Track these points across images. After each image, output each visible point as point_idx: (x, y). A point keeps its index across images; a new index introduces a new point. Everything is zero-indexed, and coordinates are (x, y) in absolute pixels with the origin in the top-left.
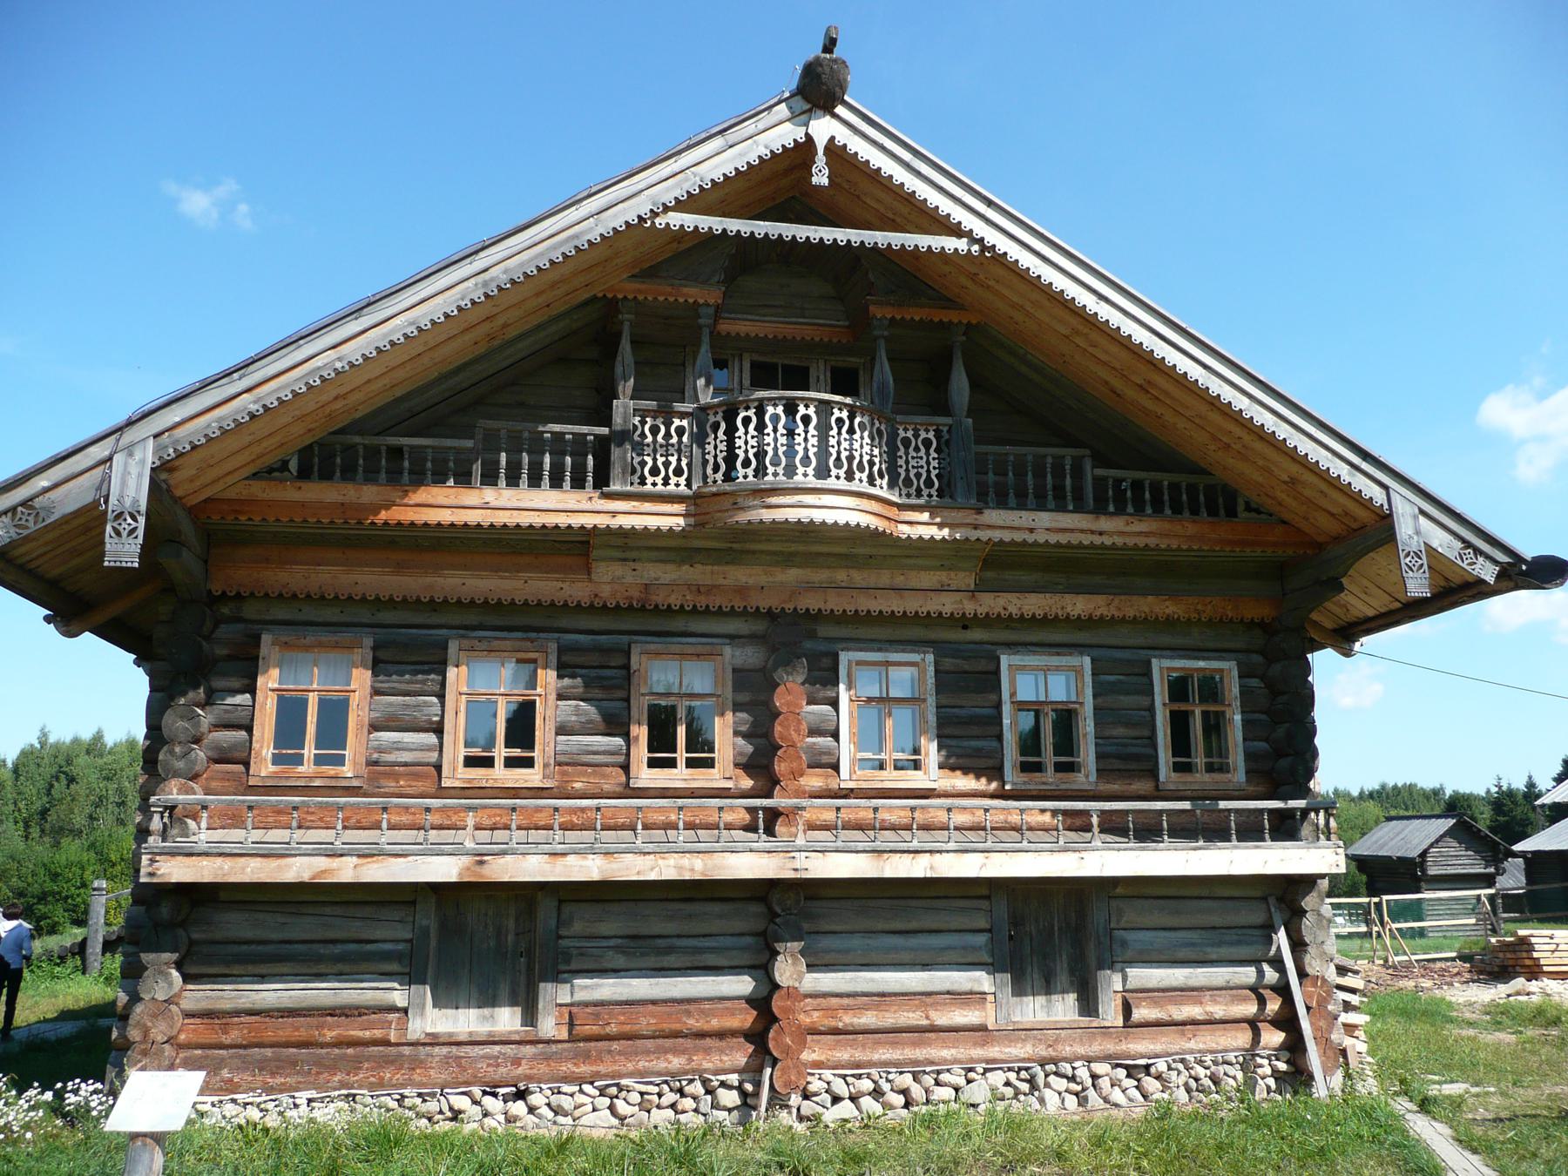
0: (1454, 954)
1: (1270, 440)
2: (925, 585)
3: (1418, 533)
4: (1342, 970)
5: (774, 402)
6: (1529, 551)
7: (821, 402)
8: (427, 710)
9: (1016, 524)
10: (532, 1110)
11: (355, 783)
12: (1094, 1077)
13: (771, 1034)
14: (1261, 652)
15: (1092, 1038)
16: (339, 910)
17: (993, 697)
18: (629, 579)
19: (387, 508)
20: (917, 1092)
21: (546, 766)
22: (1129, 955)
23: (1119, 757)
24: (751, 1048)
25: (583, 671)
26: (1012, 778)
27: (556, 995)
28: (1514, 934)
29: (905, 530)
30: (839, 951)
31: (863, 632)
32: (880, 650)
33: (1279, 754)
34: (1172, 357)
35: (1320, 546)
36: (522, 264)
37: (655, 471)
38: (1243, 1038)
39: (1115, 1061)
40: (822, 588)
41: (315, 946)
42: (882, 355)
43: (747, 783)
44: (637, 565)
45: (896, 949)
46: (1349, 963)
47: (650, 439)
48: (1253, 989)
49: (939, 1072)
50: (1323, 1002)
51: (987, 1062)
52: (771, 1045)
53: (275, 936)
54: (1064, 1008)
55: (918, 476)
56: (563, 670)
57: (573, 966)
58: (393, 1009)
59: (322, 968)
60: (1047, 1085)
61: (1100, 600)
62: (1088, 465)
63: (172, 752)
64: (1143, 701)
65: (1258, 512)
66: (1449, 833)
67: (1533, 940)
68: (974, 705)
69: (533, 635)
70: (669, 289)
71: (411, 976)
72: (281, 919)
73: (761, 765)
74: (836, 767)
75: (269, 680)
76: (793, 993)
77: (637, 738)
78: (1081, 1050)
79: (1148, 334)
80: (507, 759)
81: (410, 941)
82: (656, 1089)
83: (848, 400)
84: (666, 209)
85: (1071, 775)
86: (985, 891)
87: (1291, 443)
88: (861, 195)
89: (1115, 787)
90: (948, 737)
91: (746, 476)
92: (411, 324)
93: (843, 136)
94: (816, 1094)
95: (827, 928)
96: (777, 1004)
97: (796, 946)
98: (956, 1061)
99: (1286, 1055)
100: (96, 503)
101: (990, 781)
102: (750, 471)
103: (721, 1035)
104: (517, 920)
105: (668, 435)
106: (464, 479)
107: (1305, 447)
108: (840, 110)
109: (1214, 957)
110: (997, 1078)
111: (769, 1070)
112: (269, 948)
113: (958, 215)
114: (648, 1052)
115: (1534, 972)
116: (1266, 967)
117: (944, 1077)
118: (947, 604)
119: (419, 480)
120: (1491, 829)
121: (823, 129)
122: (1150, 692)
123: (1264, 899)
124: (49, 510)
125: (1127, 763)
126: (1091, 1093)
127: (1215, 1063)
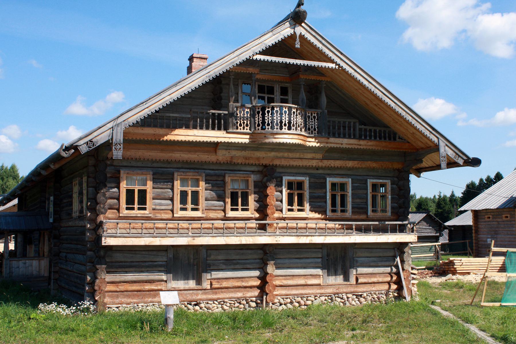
0: (424, 267)
1: (410, 124)
2: (309, 157)
3: (445, 151)
4: (412, 269)
5: (277, 107)
6: (471, 156)
7: (289, 107)
8: (168, 194)
9: (338, 142)
10: (201, 308)
11: (150, 215)
12: (348, 298)
13: (266, 287)
14: (397, 178)
15: (348, 287)
16: (147, 253)
17: (324, 190)
18: (227, 155)
19: (166, 135)
20: (302, 302)
21: (203, 210)
22: (358, 264)
23: (357, 208)
24: (259, 291)
25: (211, 182)
26: (329, 213)
27: (207, 277)
28: (448, 259)
29: (308, 144)
30: (282, 264)
31: (289, 171)
32: (293, 176)
33: (400, 207)
34: (387, 100)
35: (417, 150)
36: (219, 71)
37: (240, 125)
38: (386, 287)
39: (353, 293)
40: (280, 158)
41: (140, 263)
42: (302, 90)
43: (257, 215)
44: (230, 151)
45: (297, 263)
46: (414, 267)
47: (239, 115)
48: (389, 274)
49: (307, 297)
50: (408, 277)
51: (321, 294)
52: (266, 289)
53: (129, 260)
54: (340, 279)
55: (312, 127)
56: (207, 182)
57: (211, 268)
58: (162, 281)
59: (143, 269)
60: (336, 300)
61: (356, 162)
62: (357, 124)
63: (100, 207)
64: (365, 192)
65: (402, 139)
66: (424, 219)
67: (455, 261)
68: (319, 192)
69: (197, 170)
70: (244, 69)
71: (167, 272)
72: (131, 255)
73: (263, 210)
74: (281, 211)
75: (124, 186)
76: (272, 275)
77: (228, 202)
78: (345, 290)
79: (381, 93)
80: (192, 208)
81: (167, 261)
82: (233, 302)
83: (296, 106)
84: (257, 54)
85: (345, 213)
86: (320, 247)
87: (415, 125)
88: (309, 51)
89: (356, 217)
90: (312, 202)
91: (268, 129)
92: (190, 88)
93: (304, 32)
94: (276, 303)
95: (279, 257)
96: (268, 278)
97: (272, 262)
98: (313, 294)
99: (397, 291)
100: (109, 140)
101: (322, 215)
102: (270, 127)
103: (251, 287)
104: (194, 255)
105: (244, 114)
106: (188, 127)
107: (419, 126)
108: (303, 24)
109: (380, 265)
110: (323, 298)
111: (265, 297)
112: (128, 264)
113: (334, 57)
114: (232, 292)
115: (454, 273)
116: (393, 268)
117: (309, 298)
118: (314, 163)
119: (175, 128)
120: (435, 215)
121: (299, 30)
122: (366, 189)
123: (394, 249)
124: (97, 142)
125: (360, 210)
126: (347, 302)
127: (379, 294)
